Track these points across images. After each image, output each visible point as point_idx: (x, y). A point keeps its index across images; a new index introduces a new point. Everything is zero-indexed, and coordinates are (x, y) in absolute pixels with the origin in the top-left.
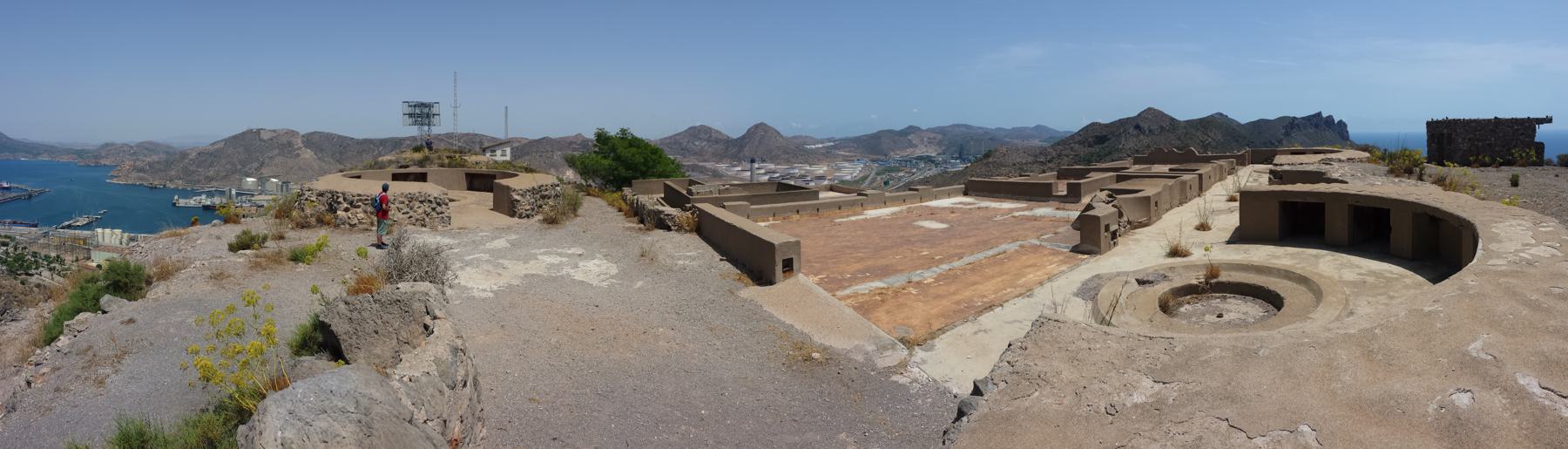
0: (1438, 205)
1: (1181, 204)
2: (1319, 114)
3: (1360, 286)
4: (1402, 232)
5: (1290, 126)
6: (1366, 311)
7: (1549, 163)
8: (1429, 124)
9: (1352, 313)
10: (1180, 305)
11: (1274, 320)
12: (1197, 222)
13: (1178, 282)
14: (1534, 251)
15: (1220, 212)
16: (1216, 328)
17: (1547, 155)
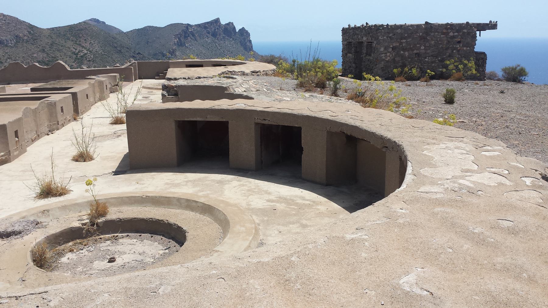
0: (358, 124)
1: (51, 131)
2: (217, 21)
3: (270, 214)
4: (314, 153)
5: (184, 34)
6: (278, 241)
7: (492, 77)
8: (345, 31)
9: (262, 244)
10: (61, 254)
11: (176, 257)
12: (74, 152)
13: (55, 227)
14: (476, 178)
15: (104, 137)
16: (105, 272)
17: (489, 68)
